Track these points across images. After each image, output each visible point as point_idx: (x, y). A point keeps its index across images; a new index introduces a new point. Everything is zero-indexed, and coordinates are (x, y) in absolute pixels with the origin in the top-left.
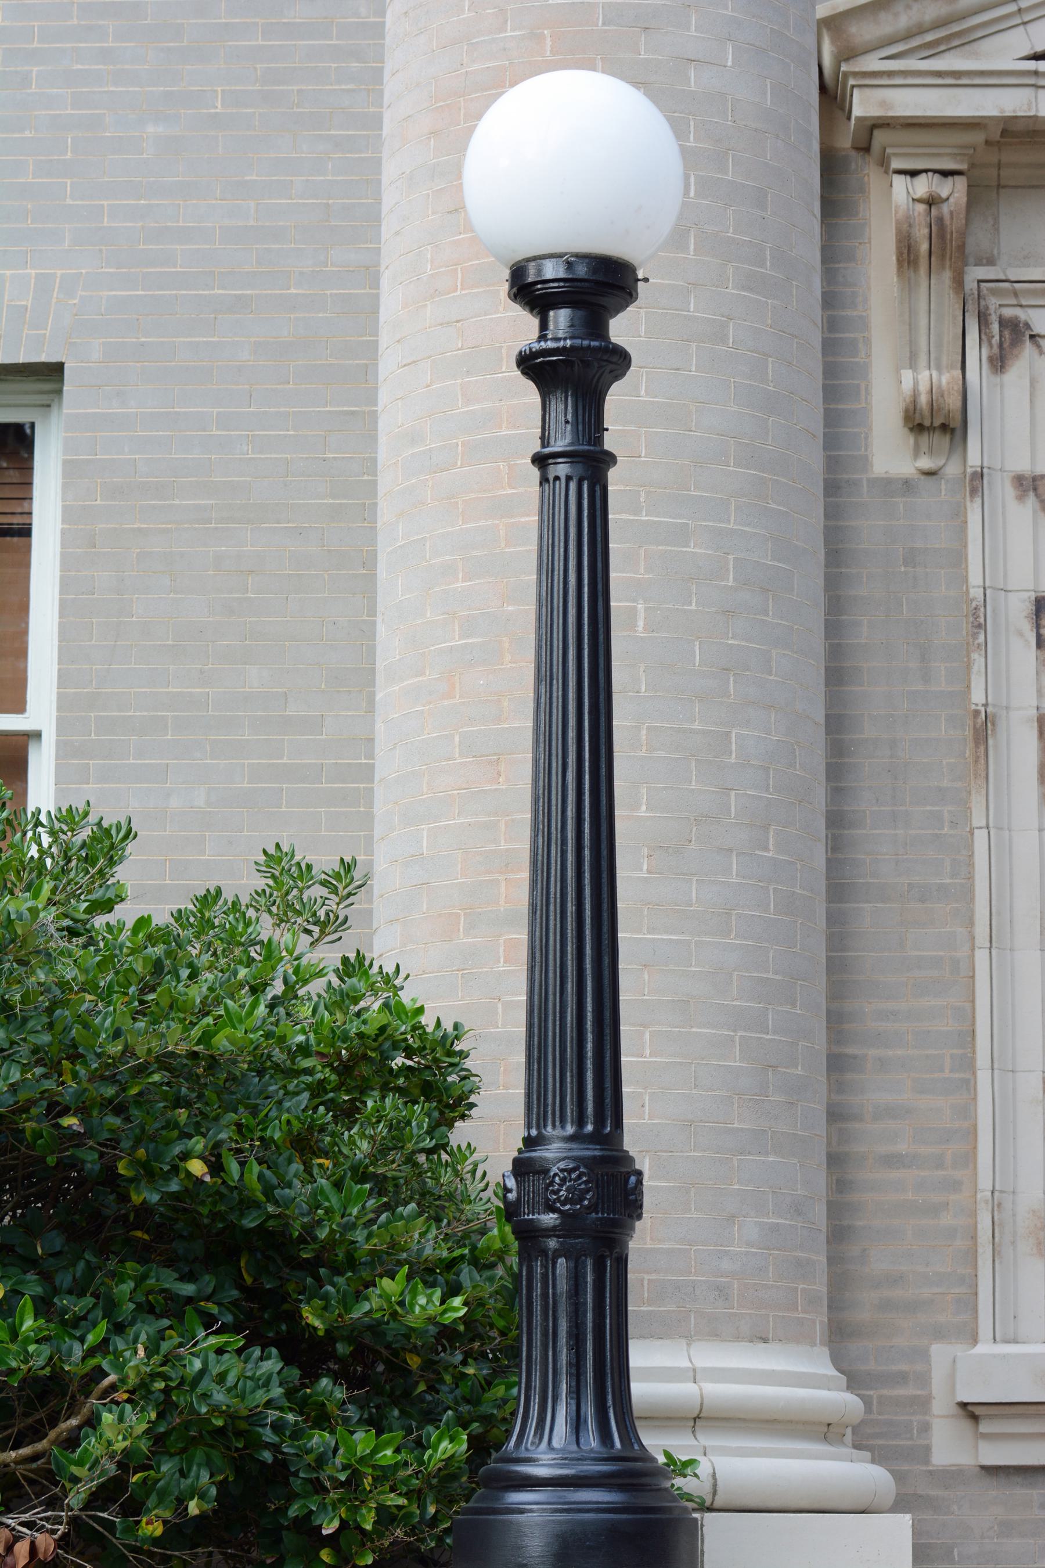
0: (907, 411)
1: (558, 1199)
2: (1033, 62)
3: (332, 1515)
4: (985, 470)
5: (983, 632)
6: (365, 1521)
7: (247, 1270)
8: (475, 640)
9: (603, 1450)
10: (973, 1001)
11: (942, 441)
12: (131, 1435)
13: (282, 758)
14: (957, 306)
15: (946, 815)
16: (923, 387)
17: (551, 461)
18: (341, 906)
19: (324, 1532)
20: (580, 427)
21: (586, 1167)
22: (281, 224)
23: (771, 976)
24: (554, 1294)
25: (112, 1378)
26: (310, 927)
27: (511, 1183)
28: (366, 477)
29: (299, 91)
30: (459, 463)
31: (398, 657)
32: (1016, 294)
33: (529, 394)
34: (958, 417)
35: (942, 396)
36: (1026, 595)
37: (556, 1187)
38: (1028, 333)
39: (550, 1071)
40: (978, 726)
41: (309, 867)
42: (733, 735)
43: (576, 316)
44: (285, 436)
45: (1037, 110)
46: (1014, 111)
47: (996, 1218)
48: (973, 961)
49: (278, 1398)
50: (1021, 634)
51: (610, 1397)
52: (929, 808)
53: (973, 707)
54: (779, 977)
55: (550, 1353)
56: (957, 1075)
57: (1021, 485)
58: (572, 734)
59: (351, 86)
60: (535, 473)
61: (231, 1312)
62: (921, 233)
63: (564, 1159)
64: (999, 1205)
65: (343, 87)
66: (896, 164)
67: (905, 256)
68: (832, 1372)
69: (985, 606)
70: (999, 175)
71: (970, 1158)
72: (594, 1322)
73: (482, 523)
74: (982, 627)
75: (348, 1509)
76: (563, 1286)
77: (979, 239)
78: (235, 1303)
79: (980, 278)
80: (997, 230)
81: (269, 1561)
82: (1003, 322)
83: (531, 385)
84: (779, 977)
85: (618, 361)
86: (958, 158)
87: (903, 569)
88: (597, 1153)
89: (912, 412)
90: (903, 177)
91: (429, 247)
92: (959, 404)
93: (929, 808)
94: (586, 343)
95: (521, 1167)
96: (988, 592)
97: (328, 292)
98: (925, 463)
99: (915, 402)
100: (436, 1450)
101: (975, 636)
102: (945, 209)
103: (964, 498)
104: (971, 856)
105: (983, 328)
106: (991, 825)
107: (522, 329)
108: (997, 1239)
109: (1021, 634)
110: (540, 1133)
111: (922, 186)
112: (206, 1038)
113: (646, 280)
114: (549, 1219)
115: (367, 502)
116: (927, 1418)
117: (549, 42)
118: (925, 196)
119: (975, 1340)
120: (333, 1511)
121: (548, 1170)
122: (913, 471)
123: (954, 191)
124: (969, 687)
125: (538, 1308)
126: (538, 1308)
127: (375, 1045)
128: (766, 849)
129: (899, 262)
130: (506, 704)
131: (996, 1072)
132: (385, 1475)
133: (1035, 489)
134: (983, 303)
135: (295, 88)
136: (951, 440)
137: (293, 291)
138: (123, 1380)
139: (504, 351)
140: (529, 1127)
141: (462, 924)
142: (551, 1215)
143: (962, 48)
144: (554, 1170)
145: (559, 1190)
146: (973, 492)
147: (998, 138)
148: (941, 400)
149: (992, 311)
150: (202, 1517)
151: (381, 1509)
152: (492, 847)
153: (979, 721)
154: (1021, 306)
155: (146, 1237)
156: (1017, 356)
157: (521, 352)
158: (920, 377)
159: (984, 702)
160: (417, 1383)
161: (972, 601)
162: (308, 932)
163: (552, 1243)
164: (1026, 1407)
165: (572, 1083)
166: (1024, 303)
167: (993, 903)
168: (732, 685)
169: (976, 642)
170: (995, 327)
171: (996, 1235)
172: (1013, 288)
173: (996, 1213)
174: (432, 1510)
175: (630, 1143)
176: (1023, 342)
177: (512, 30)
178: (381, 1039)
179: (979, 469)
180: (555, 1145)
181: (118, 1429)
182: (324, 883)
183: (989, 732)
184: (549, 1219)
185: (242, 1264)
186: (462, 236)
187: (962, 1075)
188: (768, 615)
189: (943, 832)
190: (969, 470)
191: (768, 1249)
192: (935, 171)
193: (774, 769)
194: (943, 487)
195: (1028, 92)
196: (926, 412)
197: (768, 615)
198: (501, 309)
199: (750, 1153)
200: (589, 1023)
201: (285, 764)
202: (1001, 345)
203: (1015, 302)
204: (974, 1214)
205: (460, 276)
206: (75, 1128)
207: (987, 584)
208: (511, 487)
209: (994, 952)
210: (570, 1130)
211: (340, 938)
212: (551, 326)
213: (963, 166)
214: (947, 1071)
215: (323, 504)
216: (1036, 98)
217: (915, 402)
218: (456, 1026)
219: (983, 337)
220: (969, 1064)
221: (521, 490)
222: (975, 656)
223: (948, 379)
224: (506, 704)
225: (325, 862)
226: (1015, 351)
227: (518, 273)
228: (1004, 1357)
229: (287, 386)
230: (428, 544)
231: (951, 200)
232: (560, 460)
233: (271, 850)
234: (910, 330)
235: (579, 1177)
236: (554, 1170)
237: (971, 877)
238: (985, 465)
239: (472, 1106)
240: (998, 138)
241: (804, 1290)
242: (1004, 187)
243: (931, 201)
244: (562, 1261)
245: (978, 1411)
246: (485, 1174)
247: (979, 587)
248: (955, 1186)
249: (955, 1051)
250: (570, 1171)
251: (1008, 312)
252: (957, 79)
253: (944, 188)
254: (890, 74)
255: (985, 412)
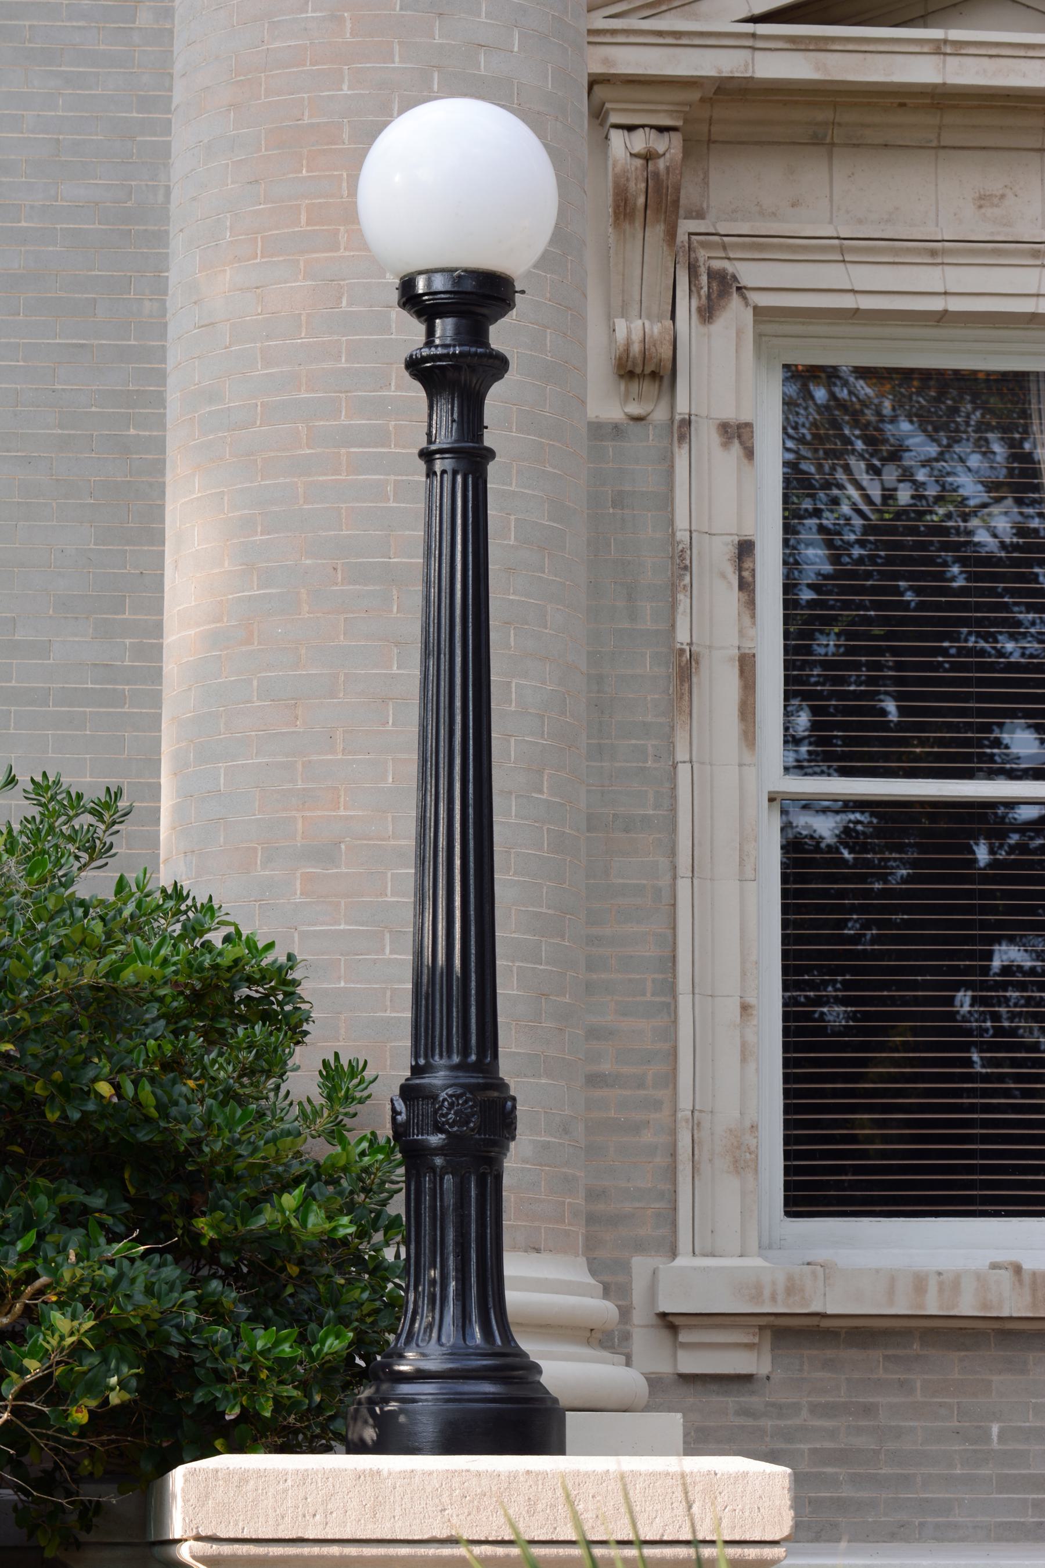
0: (620, 359)
1: (447, 1122)
2: (751, 25)
3: (233, 1402)
4: (693, 417)
5: (688, 574)
6: (264, 1409)
7: (130, 1182)
8: (274, 591)
9: (487, 1346)
10: (674, 928)
11: (649, 387)
12: (78, 1331)
13: (10, 682)
14: (669, 258)
15: (650, 749)
16: (637, 336)
17: (438, 456)
18: (108, 833)
19: (227, 1418)
20: (465, 426)
21: (471, 1093)
22: (13, 157)
23: (544, 910)
24: (441, 1206)
25: (44, 1280)
26: (81, 854)
27: (400, 1106)
28: (94, 409)
29: (30, 26)
30: (258, 423)
31: (193, 604)
32: (724, 247)
33: (417, 392)
34: (669, 365)
35: (654, 346)
36: (729, 539)
37: (445, 1111)
38: (735, 285)
39: (438, 1007)
40: (683, 664)
41: (80, 797)
42: (513, 685)
43: (461, 323)
44: (16, 366)
45: (753, 72)
46: (731, 72)
47: (696, 1137)
48: (675, 890)
49: (191, 1300)
50: (723, 576)
51: (490, 1299)
52: (633, 742)
53: (679, 646)
54: (550, 912)
55: (438, 1260)
56: (658, 999)
57: (726, 432)
58: (458, 704)
59: (81, 24)
60: (422, 466)
61: (123, 1223)
62: (637, 188)
63: (451, 1086)
64: (699, 1124)
65: (75, 24)
66: (614, 119)
67: (621, 209)
68: (590, 1280)
69: (691, 549)
70: (710, 131)
71: (671, 1078)
72: (477, 1232)
73: (281, 480)
74: (689, 568)
75: (249, 1399)
76: (450, 1200)
77: (689, 194)
78: (125, 1215)
79: (692, 230)
80: (707, 184)
81: (165, 1445)
82: (712, 274)
83: (418, 385)
84: (550, 912)
85: (498, 365)
86: (675, 114)
87: (611, 510)
88: (481, 1081)
89: (624, 359)
90: (620, 131)
91: (228, 215)
92: (671, 353)
93: (633, 742)
94: (473, 349)
95: (408, 1092)
96: (694, 535)
97: (58, 226)
98: (635, 409)
99: (627, 350)
100: (323, 1344)
101: (681, 577)
102: (661, 164)
103: (671, 444)
104: (674, 789)
105: (693, 279)
106: (694, 759)
107: (409, 334)
108: (696, 1157)
109: (723, 576)
110: (427, 1063)
111: (639, 141)
112: (114, 972)
113: (523, 292)
114: (436, 1139)
115: (95, 434)
116: (628, 1327)
117: (348, 25)
118: (643, 152)
119: (674, 1254)
120: (235, 1399)
121: (438, 1096)
122: (622, 416)
123: (669, 147)
124: (673, 626)
125: (427, 1220)
126: (427, 1220)
127: (229, 975)
128: (541, 792)
129: (616, 214)
130: (303, 651)
131: (697, 996)
132: (284, 1364)
133: (739, 437)
134: (693, 255)
135: (27, 23)
136: (660, 386)
137: (23, 224)
138: (58, 1281)
139: (303, 318)
140: (416, 1055)
141: (259, 858)
142: (440, 1136)
143: (682, 8)
144: (443, 1095)
145: (447, 1114)
146: (681, 438)
147: (711, 95)
148: (653, 350)
149: (701, 263)
150: (123, 1406)
151: (277, 1400)
152: (290, 786)
153: (684, 659)
154: (729, 259)
155: (20, 1150)
156: (724, 307)
157: (411, 356)
158: (632, 326)
159: (689, 641)
160: (285, 1286)
161: (678, 543)
162: (77, 858)
163: (439, 1161)
164: (724, 1318)
165: (458, 1017)
166: (732, 256)
167: (696, 834)
168: (512, 639)
169: (682, 583)
170: (704, 279)
171: (696, 1152)
172: (722, 242)
173: (696, 1132)
174: (317, 1398)
175: (506, 1069)
176: (729, 294)
177: (314, 11)
178: (234, 970)
179: (687, 417)
180: (442, 1073)
181: (66, 1326)
182: (93, 812)
183: (693, 670)
184: (436, 1139)
185: (126, 1176)
186: (262, 206)
187: (663, 999)
188: (544, 572)
189: (647, 765)
190: (678, 417)
191: (541, 1165)
192: (651, 127)
193: (549, 717)
194: (651, 432)
195: (747, 53)
196: (640, 361)
197: (544, 572)
198: (301, 277)
199: (525, 1076)
200: (473, 964)
201: (13, 687)
202: (709, 296)
203: (724, 255)
204: (674, 1132)
205: (260, 244)
206: (12, 1053)
207: (693, 528)
208: (309, 448)
209: (695, 881)
210: (456, 1059)
211: (106, 864)
212: (438, 333)
213: (679, 123)
214: (648, 995)
215: (52, 434)
216: (753, 59)
217: (627, 350)
218: (290, 957)
219: (693, 288)
220: (672, 989)
221: (319, 450)
222: (681, 597)
223: (657, 329)
224: (303, 651)
225: (94, 794)
226: (722, 303)
227: (407, 285)
228: (705, 1269)
229: (17, 318)
230: (226, 498)
231: (668, 155)
232: (447, 456)
233: (39, 779)
234: (623, 279)
235: (466, 1102)
236: (443, 1095)
237: (673, 809)
238: (693, 412)
239: (306, 1033)
240: (711, 95)
241: (569, 1203)
242: (715, 142)
243: (648, 157)
244: (448, 1179)
245: (677, 1321)
246: (288, 1092)
247: (685, 530)
248: (657, 1105)
249: (656, 976)
250: (458, 1097)
251: (717, 265)
252: (677, 39)
253: (660, 144)
254: (614, 32)
255: (694, 361)
